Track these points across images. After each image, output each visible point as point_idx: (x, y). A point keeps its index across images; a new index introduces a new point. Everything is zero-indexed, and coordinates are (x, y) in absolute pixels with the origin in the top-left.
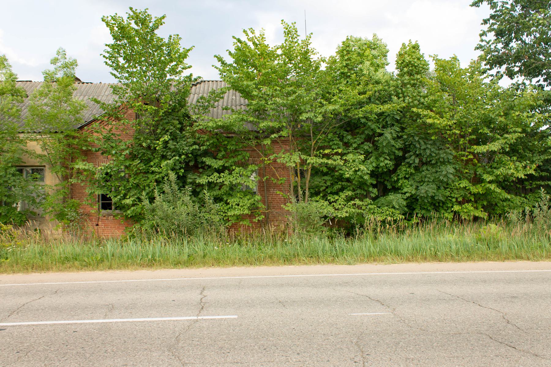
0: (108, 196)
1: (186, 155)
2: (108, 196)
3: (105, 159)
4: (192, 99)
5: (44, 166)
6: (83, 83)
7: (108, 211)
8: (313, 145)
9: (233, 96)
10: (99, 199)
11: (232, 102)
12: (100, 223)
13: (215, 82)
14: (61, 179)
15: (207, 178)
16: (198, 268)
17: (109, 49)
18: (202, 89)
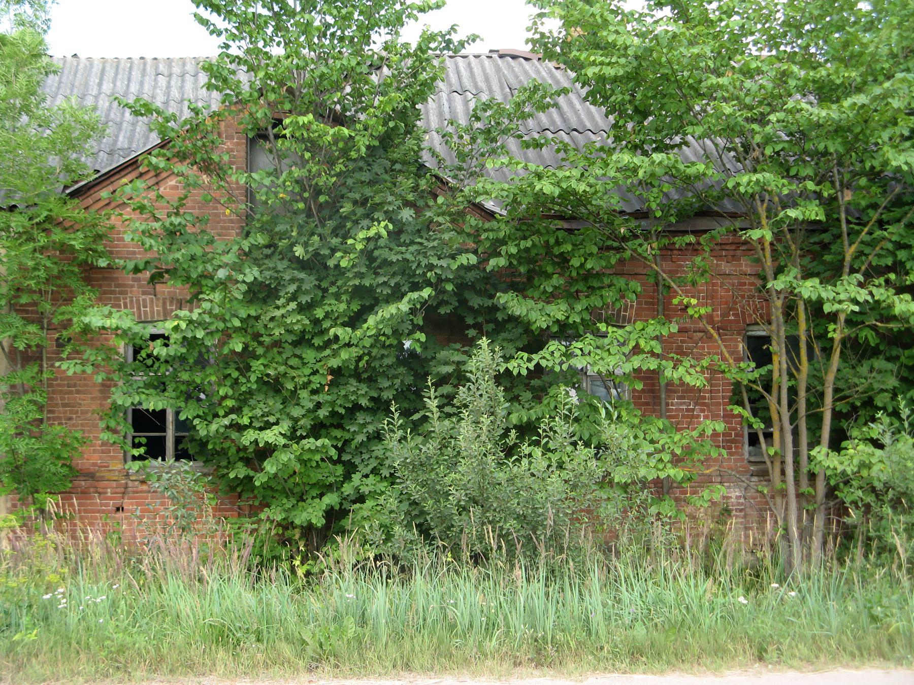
1: (437, 284)
3: (148, 298)
8: (848, 258)
12: (127, 503)
15: (530, 360)
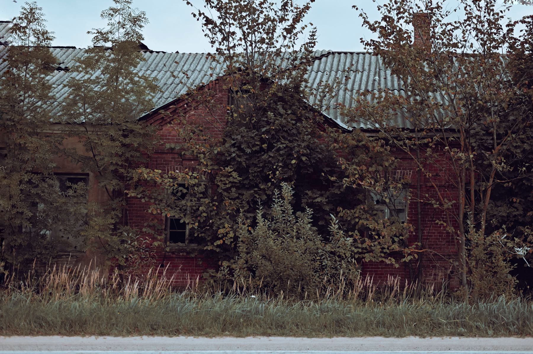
0: (182, 221)
2: (182, 221)
4: (314, 77)
5: (88, 175)
6: (152, 52)
7: (180, 244)
9: (375, 75)
10: (166, 226)
11: (373, 84)
13: (349, 55)
14: (111, 194)
16: (518, 337)
17: (375, 36)
18: (329, 64)
